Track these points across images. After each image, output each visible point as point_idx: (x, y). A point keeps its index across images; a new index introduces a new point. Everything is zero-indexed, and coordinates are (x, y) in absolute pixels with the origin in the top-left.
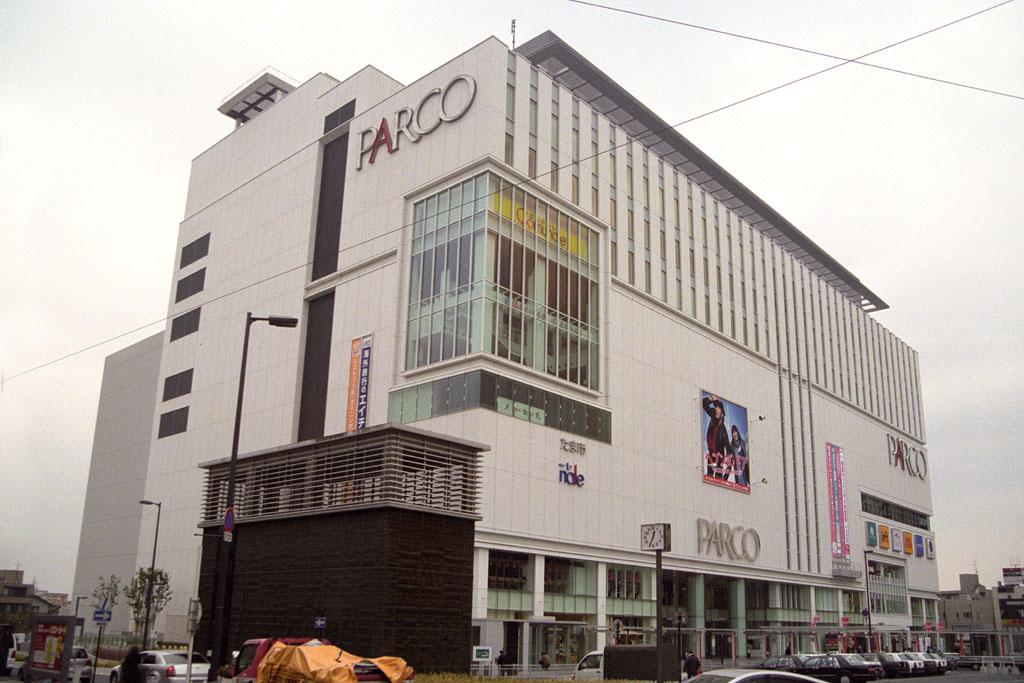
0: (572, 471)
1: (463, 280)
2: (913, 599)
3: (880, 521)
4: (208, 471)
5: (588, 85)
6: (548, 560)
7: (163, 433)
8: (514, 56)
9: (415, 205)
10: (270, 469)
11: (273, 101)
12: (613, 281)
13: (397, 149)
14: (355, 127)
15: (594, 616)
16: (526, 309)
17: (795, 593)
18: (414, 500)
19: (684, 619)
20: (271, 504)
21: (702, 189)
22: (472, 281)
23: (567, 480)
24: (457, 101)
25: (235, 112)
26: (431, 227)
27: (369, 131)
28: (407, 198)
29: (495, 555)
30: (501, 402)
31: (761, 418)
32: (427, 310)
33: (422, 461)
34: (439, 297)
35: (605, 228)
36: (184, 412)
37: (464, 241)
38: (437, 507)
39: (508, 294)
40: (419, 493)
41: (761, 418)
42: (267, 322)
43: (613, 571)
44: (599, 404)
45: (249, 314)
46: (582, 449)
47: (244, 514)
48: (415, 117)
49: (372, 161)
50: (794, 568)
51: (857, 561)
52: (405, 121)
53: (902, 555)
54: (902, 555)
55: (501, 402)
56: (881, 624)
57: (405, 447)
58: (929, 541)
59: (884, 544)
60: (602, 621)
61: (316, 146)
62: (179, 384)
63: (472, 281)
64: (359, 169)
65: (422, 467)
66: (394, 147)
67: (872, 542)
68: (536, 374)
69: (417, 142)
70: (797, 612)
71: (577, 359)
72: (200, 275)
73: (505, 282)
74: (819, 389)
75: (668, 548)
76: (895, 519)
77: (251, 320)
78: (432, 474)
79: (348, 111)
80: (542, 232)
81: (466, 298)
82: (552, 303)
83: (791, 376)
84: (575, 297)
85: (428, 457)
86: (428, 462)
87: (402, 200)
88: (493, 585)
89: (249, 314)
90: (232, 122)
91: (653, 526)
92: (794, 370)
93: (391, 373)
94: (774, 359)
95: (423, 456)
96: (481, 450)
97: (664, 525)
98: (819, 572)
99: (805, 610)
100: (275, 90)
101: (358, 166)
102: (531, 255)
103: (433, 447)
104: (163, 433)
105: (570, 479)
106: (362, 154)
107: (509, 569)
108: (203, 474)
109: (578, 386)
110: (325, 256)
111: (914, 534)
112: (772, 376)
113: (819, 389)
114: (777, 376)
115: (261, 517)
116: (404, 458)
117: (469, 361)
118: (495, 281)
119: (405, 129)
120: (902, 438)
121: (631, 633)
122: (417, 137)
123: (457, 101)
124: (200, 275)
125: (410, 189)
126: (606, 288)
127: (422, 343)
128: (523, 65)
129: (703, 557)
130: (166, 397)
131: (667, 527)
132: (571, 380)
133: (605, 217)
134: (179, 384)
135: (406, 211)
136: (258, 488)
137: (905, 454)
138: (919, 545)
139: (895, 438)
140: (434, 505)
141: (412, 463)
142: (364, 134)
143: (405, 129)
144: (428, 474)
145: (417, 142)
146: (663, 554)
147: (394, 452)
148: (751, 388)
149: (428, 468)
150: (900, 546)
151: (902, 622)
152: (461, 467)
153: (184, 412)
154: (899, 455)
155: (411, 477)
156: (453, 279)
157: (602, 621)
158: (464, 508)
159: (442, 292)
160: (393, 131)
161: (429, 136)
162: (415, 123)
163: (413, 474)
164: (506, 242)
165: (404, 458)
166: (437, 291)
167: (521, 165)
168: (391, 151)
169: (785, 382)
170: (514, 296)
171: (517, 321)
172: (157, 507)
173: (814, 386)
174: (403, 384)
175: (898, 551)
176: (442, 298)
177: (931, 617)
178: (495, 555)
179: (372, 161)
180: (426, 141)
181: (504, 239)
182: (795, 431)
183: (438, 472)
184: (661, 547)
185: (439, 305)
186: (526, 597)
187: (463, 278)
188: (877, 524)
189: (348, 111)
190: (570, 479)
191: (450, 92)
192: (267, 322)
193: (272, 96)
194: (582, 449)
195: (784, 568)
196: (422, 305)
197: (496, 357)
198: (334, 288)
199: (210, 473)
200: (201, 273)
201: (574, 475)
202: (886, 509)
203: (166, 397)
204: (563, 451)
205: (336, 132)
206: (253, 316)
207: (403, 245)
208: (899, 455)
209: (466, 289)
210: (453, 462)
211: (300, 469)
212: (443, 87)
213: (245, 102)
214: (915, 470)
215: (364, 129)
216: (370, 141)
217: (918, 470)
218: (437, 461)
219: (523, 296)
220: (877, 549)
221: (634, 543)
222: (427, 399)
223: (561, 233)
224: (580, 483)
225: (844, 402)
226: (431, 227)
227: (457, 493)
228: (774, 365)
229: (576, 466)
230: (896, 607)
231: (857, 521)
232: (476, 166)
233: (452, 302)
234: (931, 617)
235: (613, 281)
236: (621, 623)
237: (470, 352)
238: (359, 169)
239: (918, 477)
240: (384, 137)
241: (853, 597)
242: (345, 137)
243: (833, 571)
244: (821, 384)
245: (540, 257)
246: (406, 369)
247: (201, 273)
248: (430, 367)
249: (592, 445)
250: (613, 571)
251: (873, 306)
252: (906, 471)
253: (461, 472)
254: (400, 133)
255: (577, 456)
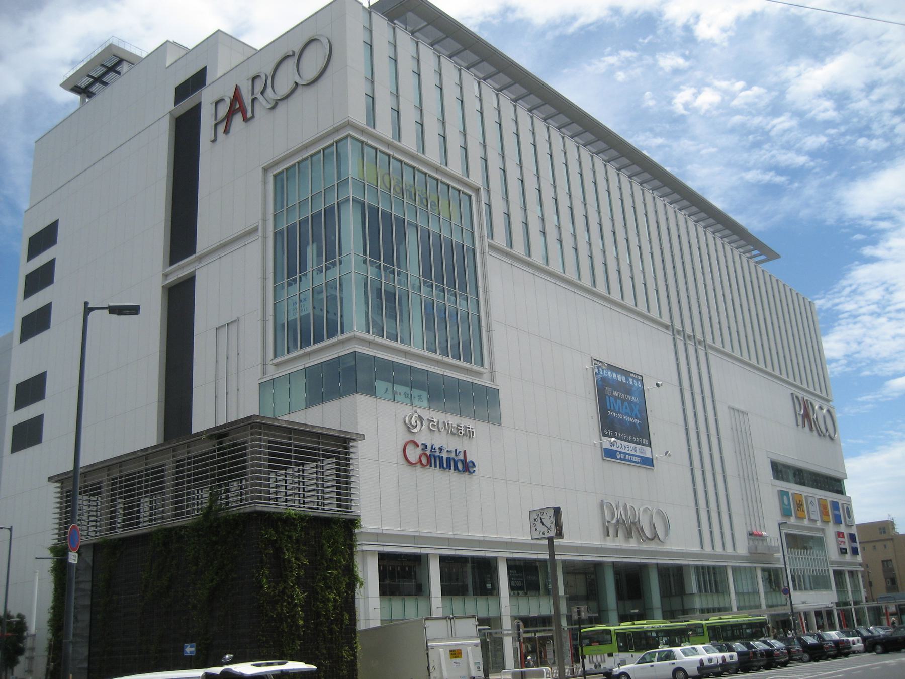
0: (461, 457)
1: (330, 255)
2: (835, 572)
3: (794, 488)
4: (59, 485)
5: (430, 26)
6: (443, 559)
7: (17, 446)
8: (370, 13)
9: (275, 176)
10: (125, 477)
11: (119, 73)
12: (490, 246)
13: (253, 117)
14: (206, 96)
15: (499, 619)
16: (399, 281)
17: (712, 578)
18: (286, 501)
19: (583, 614)
20: (131, 518)
21: (435, 49)
22: (340, 255)
23: (456, 468)
24: (312, 64)
25: (79, 87)
26: (294, 200)
27: (222, 100)
28: (266, 170)
29: (383, 557)
30: (380, 385)
31: (658, 385)
32: (295, 289)
33: (290, 457)
34: (306, 274)
35: (477, 190)
36: (38, 422)
37: (329, 211)
38: (311, 507)
39: (379, 267)
40: (292, 493)
41: (658, 385)
42: (107, 311)
43: (514, 566)
44: (485, 381)
45: (86, 304)
46: (469, 434)
47: (100, 531)
48: (269, 82)
49: (226, 131)
50: (708, 549)
51: (772, 533)
52: (259, 86)
53: (819, 524)
54: (819, 524)
55: (380, 385)
56: (804, 603)
57: (270, 442)
58: (845, 506)
59: (800, 514)
60: (507, 624)
61: (168, 117)
62: (32, 390)
63: (340, 255)
64: (214, 141)
65: (290, 463)
66: (249, 114)
67: (786, 513)
68: (414, 349)
69: (273, 108)
70: (715, 596)
71: (464, 337)
72: (50, 266)
73: (375, 254)
74: (717, 350)
75: (559, 534)
76: (809, 486)
77: (88, 310)
78: (303, 471)
79: (198, 81)
80: (411, 197)
81: (334, 273)
82: (427, 273)
83: (686, 338)
84: (453, 269)
85: (296, 452)
86: (296, 458)
87: (261, 170)
88: (385, 591)
89: (86, 304)
90: (76, 97)
91: (542, 512)
92: (689, 331)
93: (260, 360)
94: (666, 320)
95: (290, 451)
96: (354, 440)
97: (554, 508)
98: (702, 548)
99: (723, 593)
100: (120, 61)
101: (213, 138)
102: (401, 223)
103: (274, 436)
104: (17, 446)
105: (460, 466)
106: (216, 125)
107: (401, 573)
108: (54, 488)
109: (461, 363)
110: (182, 236)
111: (829, 500)
112: (666, 338)
113: (717, 350)
114: (670, 339)
115: (120, 533)
116: (270, 454)
117: (342, 342)
118: (365, 253)
119: (259, 96)
120: (807, 397)
121: (538, 635)
122: (273, 103)
123: (312, 64)
124: (50, 266)
125: (267, 162)
126: (483, 253)
127: (291, 325)
128: (380, 23)
129: (610, 543)
130: (19, 405)
131: (557, 511)
132: (442, 353)
133: (476, 178)
134: (32, 390)
135: (265, 182)
136: (115, 500)
137: (811, 414)
138: (837, 512)
139: (800, 396)
140: (326, 508)
141: (279, 459)
142: (217, 103)
143: (259, 96)
144: (299, 471)
145: (273, 108)
146: (556, 541)
147: (257, 451)
148: (646, 354)
149: (297, 465)
150: (816, 515)
151: (825, 599)
152: (334, 460)
153: (38, 422)
154: (806, 416)
155: (281, 475)
156: (319, 254)
157: (507, 624)
158: (339, 506)
159: (309, 269)
160: (247, 98)
161: (285, 101)
162: (269, 89)
163: (283, 472)
164: (374, 211)
165: (270, 454)
166: (303, 267)
167: (384, 128)
168: (246, 119)
169: (681, 345)
170: (386, 268)
171: (391, 296)
172: (8, 531)
173: (712, 348)
174: (273, 373)
175: (815, 521)
176: (310, 275)
177: (856, 589)
178: (383, 557)
179: (226, 131)
180: (282, 107)
181: (370, 207)
182: (696, 395)
183: (309, 467)
184: (552, 533)
185: (307, 285)
186: (492, 601)
187: (331, 254)
188: (791, 492)
189: (198, 81)
190: (460, 466)
191: (305, 53)
192: (107, 311)
193: (118, 69)
194: (469, 434)
195: (697, 549)
196: (289, 284)
197: (370, 337)
198: (194, 272)
199: (62, 488)
200: (51, 264)
201: (464, 462)
202: (801, 476)
203: (19, 405)
204: (450, 436)
205: (187, 104)
206: (90, 306)
207: (265, 220)
208: (806, 416)
209: (334, 264)
210: (324, 456)
211: (159, 472)
212: (297, 50)
213: (89, 76)
214: (824, 430)
215: (216, 98)
216: (223, 110)
217: (827, 430)
218: (306, 456)
219: (396, 269)
220: (792, 520)
221: (522, 534)
222: (300, 393)
223: (432, 197)
224: (471, 470)
225: (639, 314)
226: (294, 200)
227: (330, 490)
228: (667, 327)
229: (465, 452)
230: (819, 583)
231: (769, 489)
232: (337, 130)
233: (321, 280)
234: (856, 589)
235: (490, 246)
236: (521, 623)
237: (342, 333)
238: (214, 141)
239: (828, 438)
240: (237, 106)
241: (773, 579)
242: (197, 108)
243: (749, 548)
244: (718, 345)
245: (410, 224)
246: (275, 356)
247: (51, 264)
248: (302, 352)
249: (479, 428)
250: (514, 566)
251: (763, 257)
252: (815, 432)
253: (334, 466)
254: (254, 100)
255: (465, 440)
